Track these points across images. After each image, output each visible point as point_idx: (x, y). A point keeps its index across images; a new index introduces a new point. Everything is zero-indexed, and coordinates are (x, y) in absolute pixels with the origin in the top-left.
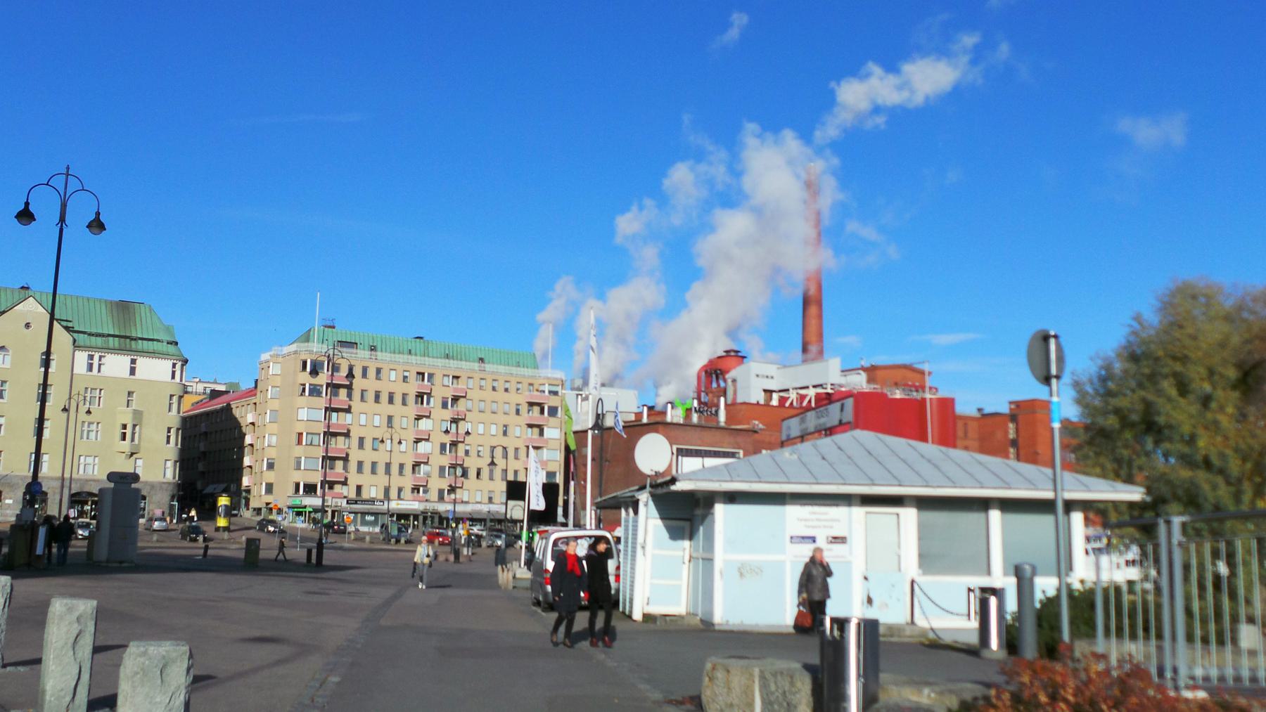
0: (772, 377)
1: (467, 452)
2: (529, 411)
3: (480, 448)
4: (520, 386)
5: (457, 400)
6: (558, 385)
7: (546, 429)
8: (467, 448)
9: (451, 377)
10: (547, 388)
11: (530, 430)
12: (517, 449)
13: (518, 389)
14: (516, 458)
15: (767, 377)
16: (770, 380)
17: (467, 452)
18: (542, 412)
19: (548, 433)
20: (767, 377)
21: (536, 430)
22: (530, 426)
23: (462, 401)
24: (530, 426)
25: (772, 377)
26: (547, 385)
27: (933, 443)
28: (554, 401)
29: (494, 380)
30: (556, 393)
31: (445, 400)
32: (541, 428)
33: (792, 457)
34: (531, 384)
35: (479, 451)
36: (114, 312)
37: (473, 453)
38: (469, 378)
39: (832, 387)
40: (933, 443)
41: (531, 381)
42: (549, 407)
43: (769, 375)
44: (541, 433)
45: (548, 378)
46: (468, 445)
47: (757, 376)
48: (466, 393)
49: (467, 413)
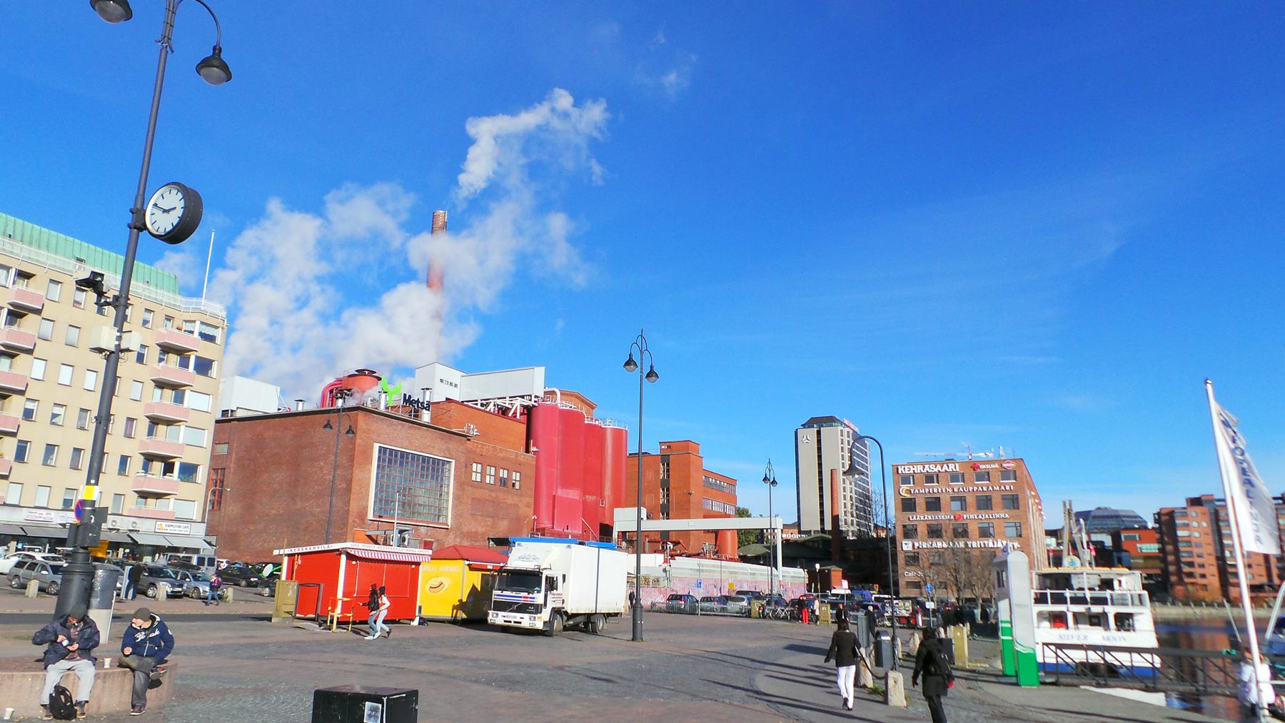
0: (456, 386)
1: (28, 414)
2: (161, 360)
3: (57, 410)
4: (149, 316)
5: (22, 316)
6: (217, 327)
7: (188, 393)
8: (30, 405)
9: (13, 272)
10: (197, 328)
11: (158, 391)
12: (130, 420)
13: (145, 322)
14: (128, 435)
15: (451, 384)
16: (452, 388)
17: (28, 414)
18: (184, 364)
19: (191, 399)
20: (451, 384)
21: (169, 393)
22: (161, 385)
23: (30, 320)
24: (161, 385)
25: (456, 386)
26: (198, 323)
27: (1052, 603)
28: (205, 350)
29: (147, 310)
30: (211, 339)
31: (1057, 553)
32: (177, 389)
33: (827, 665)
34: (169, 318)
35: (54, 416)
36: (1071, 661)
37: (42, 415)
38: (52, 281)
39: (536, 399)
40: (1052, 603)
41: (171, 313)
42: (197, 357)
43: (454, 382)
44: (179, 399)
45: (204, 313)
46: (34, 400)
47: (442, 381)
48: (43, 305)
49: (39, 343)
